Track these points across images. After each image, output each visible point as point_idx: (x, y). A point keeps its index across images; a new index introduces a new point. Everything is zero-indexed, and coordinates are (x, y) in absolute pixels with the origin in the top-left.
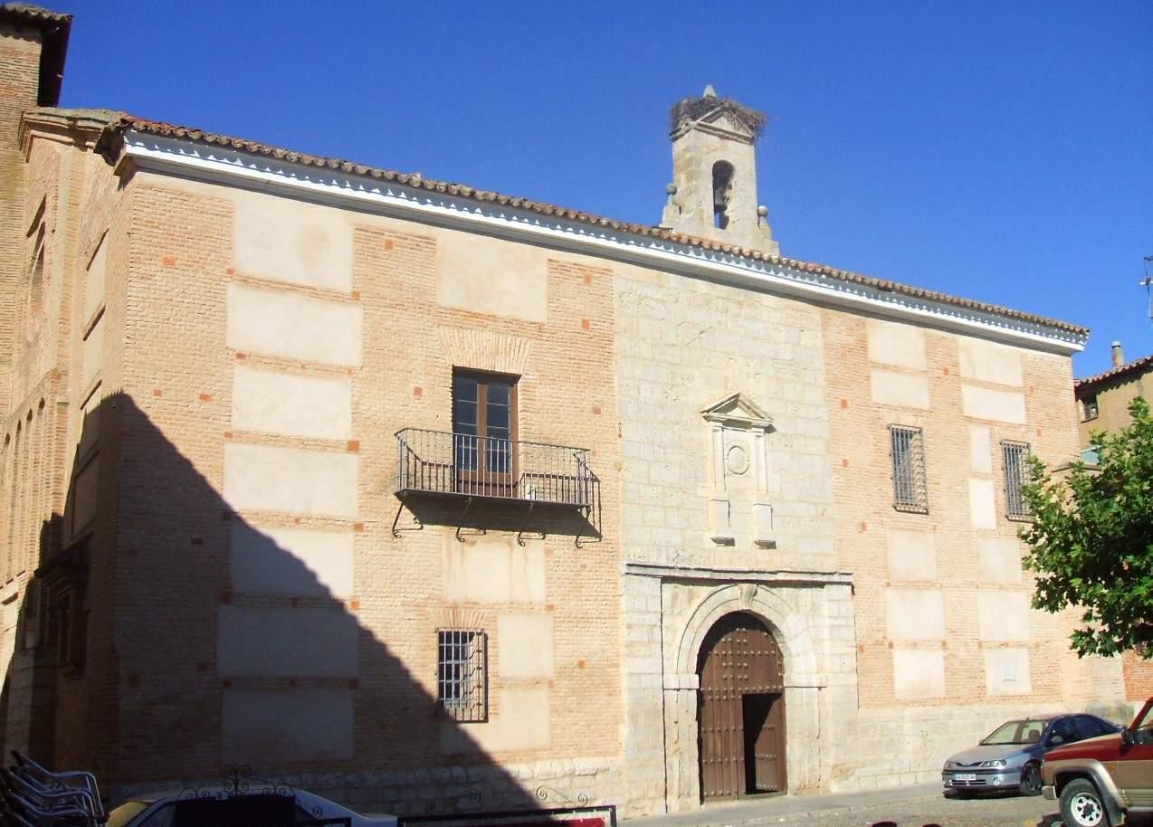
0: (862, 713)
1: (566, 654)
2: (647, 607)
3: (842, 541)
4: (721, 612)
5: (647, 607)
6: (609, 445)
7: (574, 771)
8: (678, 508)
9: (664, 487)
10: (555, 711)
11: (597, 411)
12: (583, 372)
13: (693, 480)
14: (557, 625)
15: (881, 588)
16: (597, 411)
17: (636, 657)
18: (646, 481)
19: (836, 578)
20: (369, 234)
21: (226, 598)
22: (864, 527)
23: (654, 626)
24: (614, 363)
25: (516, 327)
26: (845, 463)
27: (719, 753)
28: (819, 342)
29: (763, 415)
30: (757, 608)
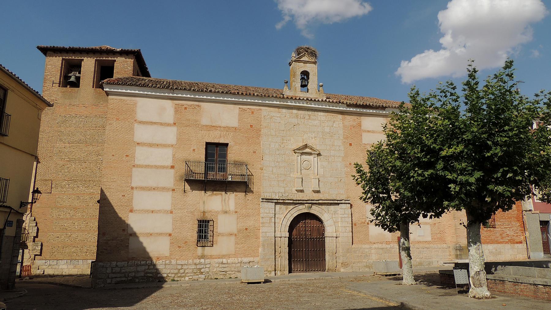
6: (259, 163)
10: (237, 243)
13: (289, 172)
16: (254, 152)
18: (272, 173)
19: (343, 202)
21: (131, 211)
25: (228, 129)
28: (341, 125)
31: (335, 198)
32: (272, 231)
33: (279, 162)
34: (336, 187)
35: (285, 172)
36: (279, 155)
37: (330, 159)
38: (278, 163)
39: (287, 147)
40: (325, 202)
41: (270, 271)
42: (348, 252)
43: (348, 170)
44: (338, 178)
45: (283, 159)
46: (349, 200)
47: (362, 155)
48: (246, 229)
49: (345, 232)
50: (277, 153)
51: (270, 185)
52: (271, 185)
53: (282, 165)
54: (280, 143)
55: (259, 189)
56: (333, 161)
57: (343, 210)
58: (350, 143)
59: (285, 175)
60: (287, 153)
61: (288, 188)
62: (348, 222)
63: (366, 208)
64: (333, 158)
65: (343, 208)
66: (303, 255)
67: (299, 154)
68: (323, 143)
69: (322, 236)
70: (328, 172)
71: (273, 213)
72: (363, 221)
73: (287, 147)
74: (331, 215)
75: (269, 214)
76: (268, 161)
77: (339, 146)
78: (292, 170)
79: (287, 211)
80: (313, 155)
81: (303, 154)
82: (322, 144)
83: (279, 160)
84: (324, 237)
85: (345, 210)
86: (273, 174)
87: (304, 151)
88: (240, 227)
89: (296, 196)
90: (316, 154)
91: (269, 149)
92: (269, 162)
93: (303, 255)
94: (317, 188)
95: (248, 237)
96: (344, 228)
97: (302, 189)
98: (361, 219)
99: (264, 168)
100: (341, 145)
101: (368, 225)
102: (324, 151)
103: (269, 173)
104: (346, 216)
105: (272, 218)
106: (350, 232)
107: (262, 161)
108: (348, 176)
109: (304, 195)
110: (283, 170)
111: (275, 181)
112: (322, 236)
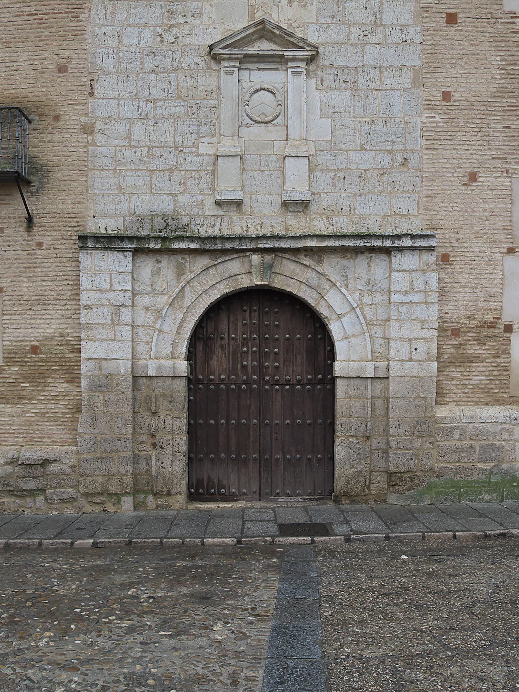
0: (441, 412)
1: (19, 339)
2: (111, 285)
3: (360, 177)
4: (223, 290)
5: (111, 285)
6: (77, 107)
7: (18, 459)
8: (171, 171)
9: (150, 148)
11: (62, 69)
12: (45, 28)
13: (194, 136)
14: (5, 308)
15: (498, 256)
16: (62, 69)
17: (95, 341)
18: (126, 143)
19: (407, 242)
20: (51, 20)
22: (473, 177)
23: (123, 305)
24: (86, 11)
26: (447, 96)
27: (233, 448)
29: (301, 44)
30: (278, 283)
31: (375, 230)
32: (124, 356)
33: (155, 101)
34: (380, 189)
35: (179, 139)
36: (153, 75)
37: (361, 80)
38: (150, 105)
39: (187, 40)
40: (331, 243)
41: (116, 494)
42: (416, 433)
43: (437, 122)
44: (390, 152)
45: (172, 89)
46: (433, 236)
47: (498, 58)
48: (35, 349)
49: (411, 360)
50: (149, 65)
51: (120, 188)
52: (124, 186)
53: (168, 110)
54: (159, 30)
55: (79, 203)
56: (373, 85)
57: (407, 275)
58: (448, 11)
59: (176, 148)
60: (185, 64)
61: (189, 196)
62: (423, 322)
63: (502, 271)
64: (374, 74)
65: (404, 268)
66: (258, 655)
67: (232, 64)
68: (333, 17)
69: (325, 376)
70: (351, 132)
71: (125, 291)
72: (490, 317)
73: (187, 40)
74: (357, 296)
75: (111, 295)
76: (114, 98)
77: (403, 28)
78: (203, 129)
79: (178, 282)
80: (290, 64)
81: (247, 58)
82: (329, 20)
83: (155, 93)
84: (329, 377)
85: (414, 275)
86: (130, 146)
87: (252, 50)
88: (10, 341)
89: (217, 227)
90: (302, 60)
91: (117, 54)
92: (115, 101)
93: (258, 655)
94: (300, 192)
95: (42, 376)
96: (406, 345)
97: (238, 195)
98: (479, 310)
99: (99, 125)
100: (411, 22)
101: (508, 335)
102: (336, 49)
103: (116, 142)
104: (416, 298)
105: (123, 310)
106: (429, 360)
107: (90, 100)
108: (435, 147)
109: (250, 221)
110: (172, 131)
111: (139, 173)
112: (325, 376)
